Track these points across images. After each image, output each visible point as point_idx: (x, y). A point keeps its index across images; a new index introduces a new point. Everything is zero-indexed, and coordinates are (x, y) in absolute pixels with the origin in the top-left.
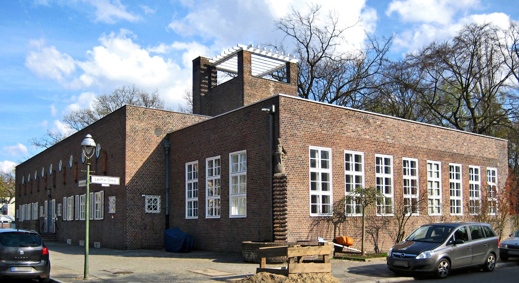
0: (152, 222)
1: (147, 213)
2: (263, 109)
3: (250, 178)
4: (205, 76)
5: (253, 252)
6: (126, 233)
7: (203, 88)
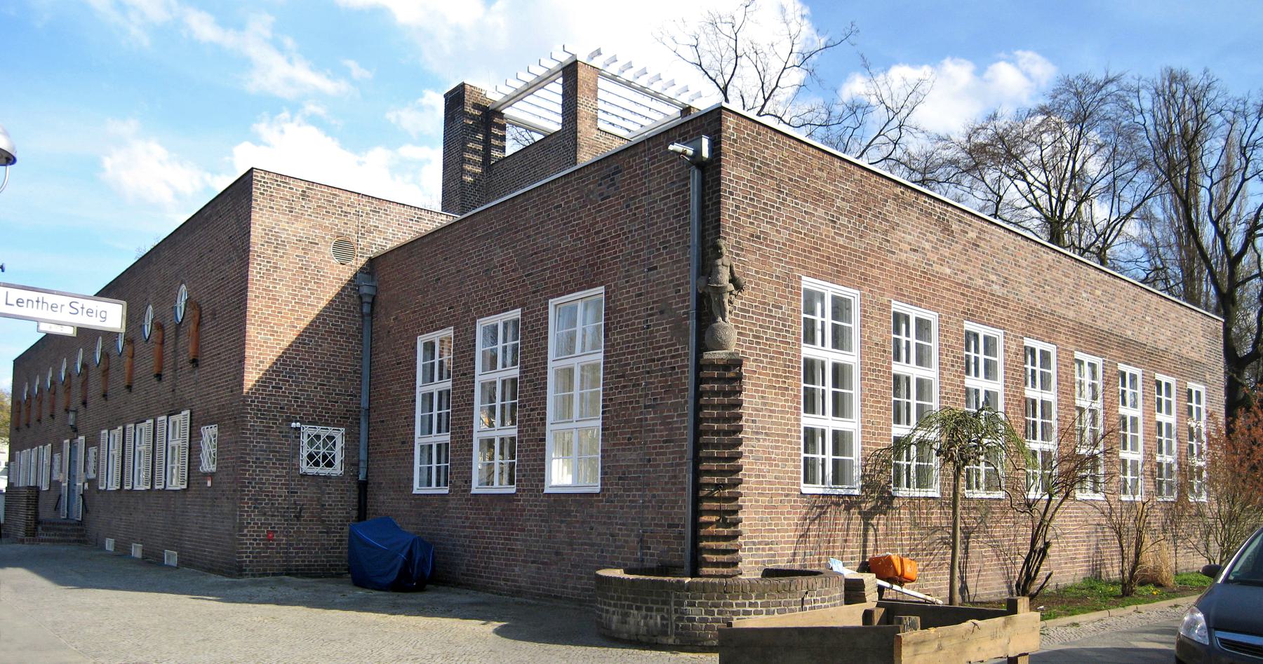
0: (319, 499)
1: (304, 475)
2: (671, 148)
3: (617, 373)
4: (477, 132)
5: (638, 608)
6: (241, 530)
7: (469, 161)
